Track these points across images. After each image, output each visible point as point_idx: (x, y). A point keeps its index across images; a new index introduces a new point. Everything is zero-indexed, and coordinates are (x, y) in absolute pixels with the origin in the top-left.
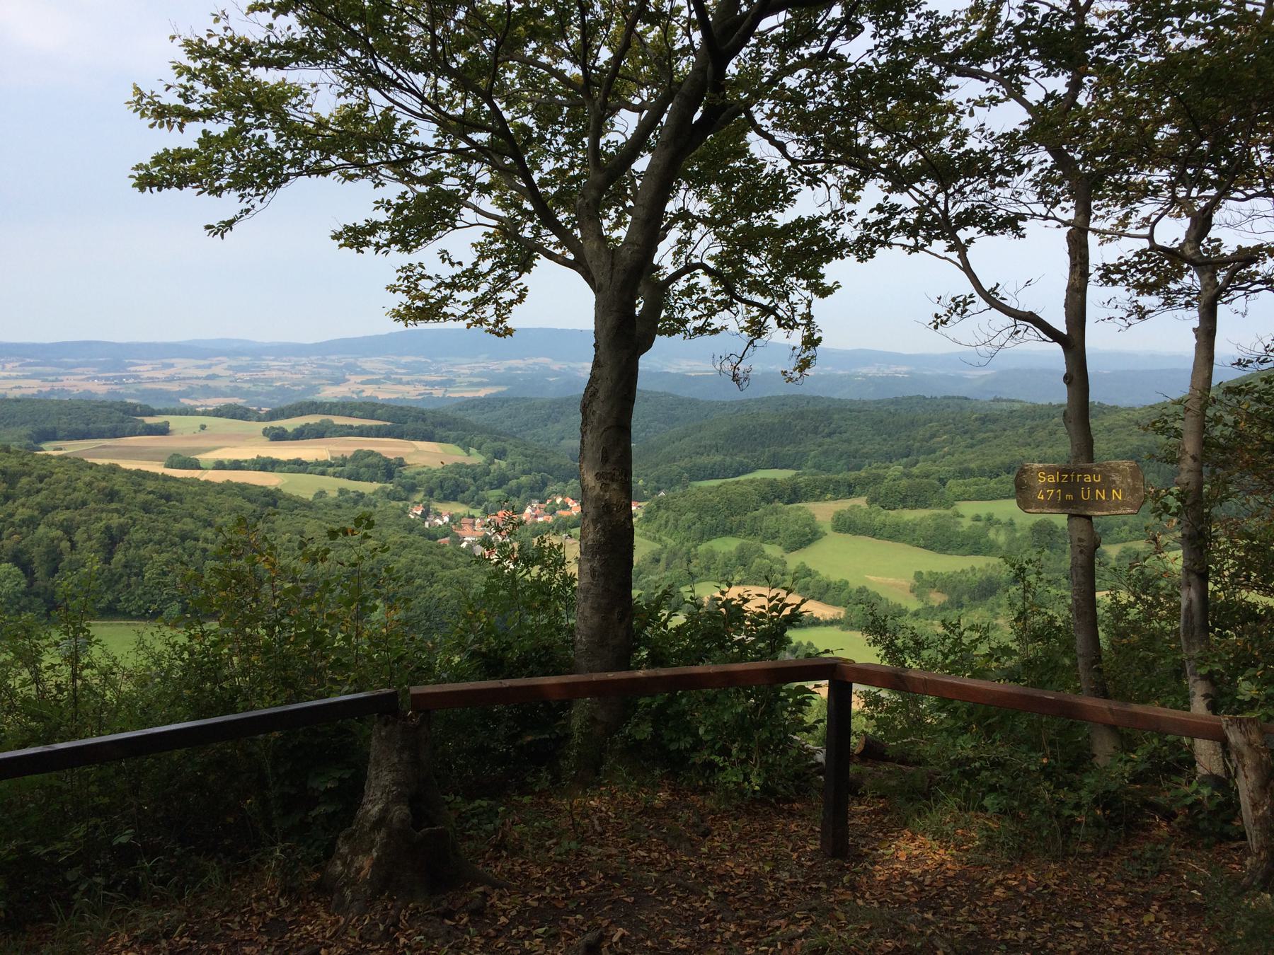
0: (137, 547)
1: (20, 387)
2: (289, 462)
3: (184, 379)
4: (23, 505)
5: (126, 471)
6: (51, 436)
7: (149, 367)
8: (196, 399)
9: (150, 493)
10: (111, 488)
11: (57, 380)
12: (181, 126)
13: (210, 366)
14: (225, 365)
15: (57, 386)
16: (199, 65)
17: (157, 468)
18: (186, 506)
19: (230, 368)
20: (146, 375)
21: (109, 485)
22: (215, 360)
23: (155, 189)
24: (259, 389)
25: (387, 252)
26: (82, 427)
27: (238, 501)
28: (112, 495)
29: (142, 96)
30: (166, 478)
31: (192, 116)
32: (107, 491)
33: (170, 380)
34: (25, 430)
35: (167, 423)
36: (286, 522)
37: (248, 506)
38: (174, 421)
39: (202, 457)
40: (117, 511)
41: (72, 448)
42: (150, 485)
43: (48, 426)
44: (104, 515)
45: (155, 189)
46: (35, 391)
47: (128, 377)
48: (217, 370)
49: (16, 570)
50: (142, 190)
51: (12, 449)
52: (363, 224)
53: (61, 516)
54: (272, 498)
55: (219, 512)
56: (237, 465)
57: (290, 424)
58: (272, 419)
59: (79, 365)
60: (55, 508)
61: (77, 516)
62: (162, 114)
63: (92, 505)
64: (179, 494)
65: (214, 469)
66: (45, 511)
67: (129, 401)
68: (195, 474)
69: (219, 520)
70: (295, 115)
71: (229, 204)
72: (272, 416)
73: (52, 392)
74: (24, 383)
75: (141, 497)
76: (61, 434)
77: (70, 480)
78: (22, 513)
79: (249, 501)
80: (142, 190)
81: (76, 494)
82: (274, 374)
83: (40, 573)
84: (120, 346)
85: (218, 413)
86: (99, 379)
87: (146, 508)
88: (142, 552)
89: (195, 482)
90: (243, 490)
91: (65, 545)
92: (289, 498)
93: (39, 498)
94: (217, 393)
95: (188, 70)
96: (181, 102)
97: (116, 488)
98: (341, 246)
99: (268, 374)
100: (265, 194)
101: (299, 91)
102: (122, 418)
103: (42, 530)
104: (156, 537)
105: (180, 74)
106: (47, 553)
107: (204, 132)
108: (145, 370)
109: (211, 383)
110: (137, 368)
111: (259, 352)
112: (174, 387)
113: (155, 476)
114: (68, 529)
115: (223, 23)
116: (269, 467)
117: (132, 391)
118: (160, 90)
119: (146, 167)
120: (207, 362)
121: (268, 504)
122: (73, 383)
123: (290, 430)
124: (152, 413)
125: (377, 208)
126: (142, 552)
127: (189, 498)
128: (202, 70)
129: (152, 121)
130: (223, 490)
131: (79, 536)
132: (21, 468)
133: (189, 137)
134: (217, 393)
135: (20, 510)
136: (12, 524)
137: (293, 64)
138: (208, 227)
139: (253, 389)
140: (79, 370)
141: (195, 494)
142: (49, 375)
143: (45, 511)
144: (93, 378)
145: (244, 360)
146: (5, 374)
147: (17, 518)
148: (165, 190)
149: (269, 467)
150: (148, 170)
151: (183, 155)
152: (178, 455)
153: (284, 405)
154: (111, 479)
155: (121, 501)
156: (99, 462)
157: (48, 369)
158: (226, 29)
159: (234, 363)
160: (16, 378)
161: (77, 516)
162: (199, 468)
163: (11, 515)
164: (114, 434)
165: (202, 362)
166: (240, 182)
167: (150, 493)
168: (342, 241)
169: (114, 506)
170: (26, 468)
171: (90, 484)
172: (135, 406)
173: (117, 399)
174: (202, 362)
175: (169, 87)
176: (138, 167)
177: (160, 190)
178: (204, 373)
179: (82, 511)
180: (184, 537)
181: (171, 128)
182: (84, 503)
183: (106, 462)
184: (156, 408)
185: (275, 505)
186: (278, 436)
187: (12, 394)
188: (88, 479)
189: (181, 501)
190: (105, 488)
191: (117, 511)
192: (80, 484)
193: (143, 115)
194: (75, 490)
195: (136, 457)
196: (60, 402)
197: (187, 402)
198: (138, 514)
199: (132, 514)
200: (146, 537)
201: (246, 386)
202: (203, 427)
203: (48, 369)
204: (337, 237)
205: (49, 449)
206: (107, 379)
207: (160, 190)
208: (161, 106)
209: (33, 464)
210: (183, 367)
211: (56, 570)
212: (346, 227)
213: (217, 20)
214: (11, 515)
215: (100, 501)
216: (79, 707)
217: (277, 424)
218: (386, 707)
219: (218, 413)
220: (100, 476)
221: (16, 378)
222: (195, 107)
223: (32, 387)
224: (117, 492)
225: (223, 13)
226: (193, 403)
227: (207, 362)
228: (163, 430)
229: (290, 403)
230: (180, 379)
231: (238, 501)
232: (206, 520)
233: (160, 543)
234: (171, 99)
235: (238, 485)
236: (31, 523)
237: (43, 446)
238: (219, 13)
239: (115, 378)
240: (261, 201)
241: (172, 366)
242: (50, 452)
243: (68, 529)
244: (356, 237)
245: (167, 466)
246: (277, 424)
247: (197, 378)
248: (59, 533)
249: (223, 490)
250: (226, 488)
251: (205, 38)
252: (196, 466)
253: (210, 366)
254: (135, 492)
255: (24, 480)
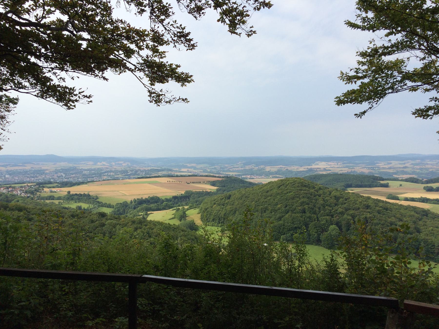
0: (375, 225)
1: (342, 170)
2: (434, 200)
3: (395, 168)
4: (340, 207)
5: (373, 199)
6: (350, 186)
7: (383, 164)
8: (399, 175)
9: (381, 207)
10: (367, 205)
11: (353, 168)
12: (355, 82)
13: (404, 164)
14: (410, 163)
15: (353, 170)
16: (366, 60)
17: (384, 199)
18: (393, 213)
19: (412, 164)
20: (382, 167)
21: (367, 203)
22: (406, 162)
23: (342, 104)
24: (423, 172)
25: (431, 118)
26: (360, 183)
27: (413, 213)
28: (368, 207)
29: (343, 74)
30: (386, 202)
31: (359, 78)
32: (366, 205)
33: (390, 168)
34: (343, 184)
35: (388, 183)
36: (431, 223)
37: (416, 215)
38: (390, 183)
39: (400, 196)
40: (369, 212)
41: (356, 190)
42: (381, 204)
43: (350, 183)
44: (365, 213)
45: (342, 104)
46: (346, 172)
47: (375, 167)
48: (407, 165)
49: (337, 228)
50: (338, 105)
51: (338, 189)
52: (424, 108)
53: (351, 212)
54: (426, 213)
55: (405, 216)
56: (413, 200)
57: (435, 185)
58: (427, 183)
59: (360, 164)
60: (350, 209)
61: (356, 212)
62: (350, 79)
63: (361, 209)
64: (390, 208)
65: (404, 200)
66: (347, 210)
67: (375, 175)
68: (397, 202)
69: (405, 219)
70: (404, 69)
71: (365, 105)
72: (427, 182)
73: (351, 172)
74: (343, 169)
75: (378, 208)
76: (353, 185)
77: (355, 201)
78: (340, 210)
79: (417, 213)
80: (338, 105)
81: (357, 205)
82: (429, 166)
83: (344, 230)
84: (374, 157)
85: (407, 180)
86: (366, 168)
87: (379, 212)
88: (376, 227)
89: (396, 204)
90: (415, 209)
91: (352, 221)
92: (433, 214)
93: (345, 206)
94: (406, 173)
95: (362, 62)
96: (355, 74)
97: (369, 204)
98: (416, 117)
99: (427, 166)
100: (378, 101)
101: (403, 61)
102: (372, 181)
103: (345, 216)
104: (382, 223)
105: (360, 64)
106: (346, 223)
107: (362, 82)
108: (382, 165)
109: (405, 170)
110: (379, 164)
111: (423, 158)
112: (391, 171)
113: (383, 201)
114: (353, 217)
115: (373, 43)
116: (425, 201)
117: (377, 172)
118: (348, 71)
119: (339, 97)
120: (403, 162)
121: (424, 215)
122: (358, 169)
123: (434, 188)
124: (383, 180)
125: (431, 101)
126: (376, 227)
127: (394, 210)
128: (366, 62)
129: (346, 82)
130: (407, 208)
131: (356, 219)
132: (340, 196)
133: (355, 86)
134: (406, 173)
135: (339, 209)
136: (337, 213)
137: (396, 52)
138: (355, 115)
139: (421, 172)
140: (360, 165)
141: (397, 209)
142: (351, 166)
143: (347, 210)
144: (364, 168)
145: (418, 161)
146: (338, 166)
147: (338, 211)
148: (346, 104)
149: (425, 201)
150: (340, 98)
151: (353, 92)
152: (391, 195)
153: (433, 178)
154: (368, 201)
155: (371, 209)
156: (364, 195)
157: (351, 165)
158: (374, 45)
159: (413, 162)
160: (341, 167)
161: (356, 212)
162: (399, 200)
163: (337, 210)
164: (370, 186)
165: (401, 162)
166: (369, 98)
167: (381, 207)
168: (416, 115)
169: (368, 210)
170: (342, 196)
171: (361, 202)
172: (377, 177)
173: (371, 175)
174: (401, 162)
175: (351, 70)
176: (336, 98)
177: (344, 104)
178: (402, 166)
179: (358, 211)
180: (391, 224)
181: (352, 83)
182: (359, 209)
183: (367, 195)
184: (384, 178)
185: (427, 216)
186: (430, 190)
187: (339, 173)
188: (360, 201)
189: (391, 211)
190: (365, 204)
191: (369, 212)
192: (358, 202)
193: (343, 80)
194: (356, 204)
195: (377, 194)
196: (353, 175)
197: (395, 176)
198: (376, 214)
199: (374, 214)
200: (378, 222)
201: (418, 171)
202: (401, 185)
203: (351, 165)
204: (414, 114)
205: (350, 190)
206: (369, 168)
207: (344, 104)
208: (349, 76)
209: (344, 194)
210: (395, 164)
211: (349, 229)
212: (416, 109)
213: (371, 43)
214: (337, 210)
215: (364, 208)
216: (292, 277)
217: (429, 185)
218: (393, 305)
219: (407, 180)
220: (364, 200)
221: (341, 167)
222: (360, 75)
223: (345, 170)
224: (370, 206)
225: (373, 40)
226: (397, 176)
227: (403, 162)
228: (386, 186)
229: (435, 177)
230: (393, 168)
231: (413, 213)
232: (400, 219)
233: (383, 225)
234: (352, 73)
235: (413, 207)
236: (342, 213)
237: (348, 189)
238: (372, 40)
239: (372, 167)
240: (376, 104)
241: (391, 163)
242: (349, 191)
243: (353, 217)
244: (423, 113)
245: (387, 198)
246: (429, 185)
247: (400, 168)
248: (350, 217)
249: (407, 208)
250: (408, 208)
251: (367, 50)
252: (397, 199)
253: (404, 164)
254: (375, 206)
255: (341, 200)
